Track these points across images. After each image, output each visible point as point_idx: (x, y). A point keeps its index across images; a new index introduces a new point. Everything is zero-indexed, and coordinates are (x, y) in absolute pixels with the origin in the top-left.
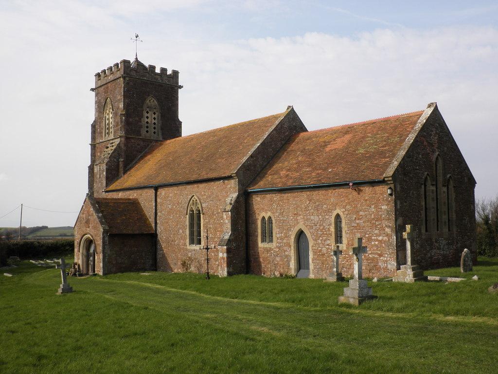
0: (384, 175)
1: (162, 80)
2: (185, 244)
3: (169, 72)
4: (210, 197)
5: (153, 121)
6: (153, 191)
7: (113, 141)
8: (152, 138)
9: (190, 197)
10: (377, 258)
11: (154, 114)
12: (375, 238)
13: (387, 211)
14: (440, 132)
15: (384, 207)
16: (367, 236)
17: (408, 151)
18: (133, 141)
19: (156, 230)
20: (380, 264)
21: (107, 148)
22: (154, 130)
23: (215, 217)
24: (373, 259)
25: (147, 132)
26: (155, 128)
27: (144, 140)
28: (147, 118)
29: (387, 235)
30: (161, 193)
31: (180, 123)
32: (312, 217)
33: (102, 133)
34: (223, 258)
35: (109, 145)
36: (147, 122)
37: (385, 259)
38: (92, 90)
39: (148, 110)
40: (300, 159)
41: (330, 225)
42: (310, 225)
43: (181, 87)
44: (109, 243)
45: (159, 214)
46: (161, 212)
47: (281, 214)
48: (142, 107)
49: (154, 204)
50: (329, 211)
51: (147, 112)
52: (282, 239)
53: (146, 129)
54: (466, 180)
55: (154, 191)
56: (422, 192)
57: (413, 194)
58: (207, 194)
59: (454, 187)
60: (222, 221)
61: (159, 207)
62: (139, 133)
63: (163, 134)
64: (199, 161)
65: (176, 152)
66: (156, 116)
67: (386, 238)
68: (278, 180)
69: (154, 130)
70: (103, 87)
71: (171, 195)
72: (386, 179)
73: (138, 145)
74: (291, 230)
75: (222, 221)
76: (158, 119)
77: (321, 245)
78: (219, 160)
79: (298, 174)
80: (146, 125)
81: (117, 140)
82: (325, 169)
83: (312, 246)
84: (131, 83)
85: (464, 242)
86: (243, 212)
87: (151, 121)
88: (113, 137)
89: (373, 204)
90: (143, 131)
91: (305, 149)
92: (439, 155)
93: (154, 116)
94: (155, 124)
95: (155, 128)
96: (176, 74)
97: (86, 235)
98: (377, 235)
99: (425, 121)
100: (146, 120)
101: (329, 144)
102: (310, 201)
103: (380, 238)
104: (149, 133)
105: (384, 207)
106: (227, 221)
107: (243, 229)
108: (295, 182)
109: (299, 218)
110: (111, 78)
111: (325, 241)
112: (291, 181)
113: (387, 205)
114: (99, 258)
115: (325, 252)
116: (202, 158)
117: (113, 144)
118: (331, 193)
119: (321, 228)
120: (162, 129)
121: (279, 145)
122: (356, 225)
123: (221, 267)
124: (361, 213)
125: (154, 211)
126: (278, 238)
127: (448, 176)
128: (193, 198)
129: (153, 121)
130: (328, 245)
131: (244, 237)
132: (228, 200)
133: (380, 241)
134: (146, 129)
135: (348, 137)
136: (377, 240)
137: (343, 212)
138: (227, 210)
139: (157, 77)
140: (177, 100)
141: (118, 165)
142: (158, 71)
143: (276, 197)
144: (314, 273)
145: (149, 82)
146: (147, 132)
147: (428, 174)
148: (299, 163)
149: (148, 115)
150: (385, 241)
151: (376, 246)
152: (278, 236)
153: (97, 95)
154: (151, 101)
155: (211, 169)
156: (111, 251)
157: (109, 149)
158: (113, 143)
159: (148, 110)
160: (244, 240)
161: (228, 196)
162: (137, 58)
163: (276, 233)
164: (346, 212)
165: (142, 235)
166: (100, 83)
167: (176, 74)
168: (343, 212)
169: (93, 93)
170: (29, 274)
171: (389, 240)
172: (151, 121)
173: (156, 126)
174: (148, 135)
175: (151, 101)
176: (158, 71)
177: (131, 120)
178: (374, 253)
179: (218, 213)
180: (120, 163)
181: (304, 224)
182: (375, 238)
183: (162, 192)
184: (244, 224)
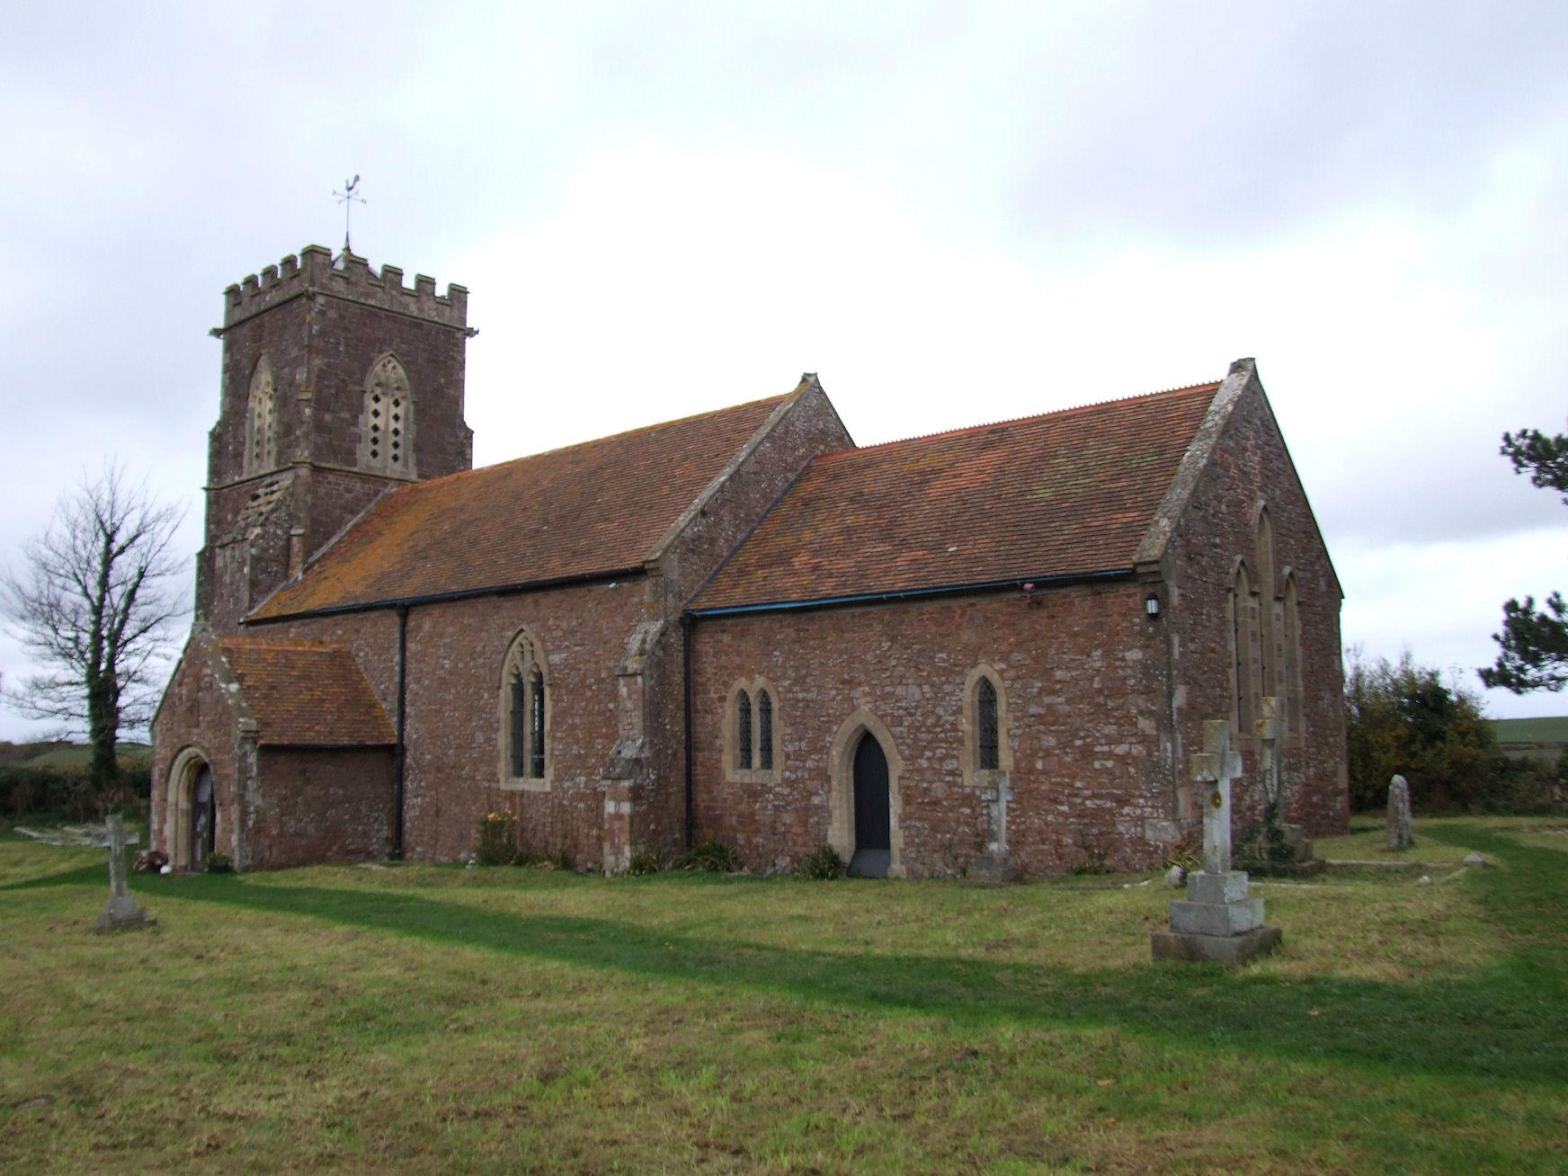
0: (1135, 558)
1: (421, 310)
2: (495, 774)
3: (441, 290)
4: (573, 632)
5: (393, 425)
6: (394, 620)
7: (275, 478)
8: (388, 473)
9: (511, 634)
10: (1110, 809)
11: (397, 403)
12: (1106, 748)
13: (1145, 666)
14: (1266, 444)
15: (1135, 655)
16: (1078, 743)
17: (1195, 490)
18: (331, 478)
19: (401, 736)
20: (1121, 828)
21: (255, 497)
22: (393, 451)
23: (589, 694)
24: (1097, 813)
25: (375, 454)
26: (396, 445)
27: (365, 477)
28: (376, 414)
29: (1144, 739)
30: (419, 627)
31: (469, 434)
32: (900, 691)
33: (241, 455)
34: (618, 816)
35: (261, 491)
36: (375, 428)
37: (1138, 811)
38: (216, 332)
39: (378, 391)
40: (850, 520)
41: (959, 711)
42: (892, 716)
43: (472, 333)
44: (260, 773)
45: (412, 686)
46: (418, 680)
47: (800, 681)
48: (361, 382)
49: (397, 658)
50: (953, 671)
51: (377, 399)
52: (801, 756)
53: (372, 447)
54: (1323, 586)
55: (397, 620)
56: (1230, 616)
57: (1208, 615)
58: (564, 625)
59: (1299, 604)
60: (611, 706)
61: (412, 667)
62: (350, 456)
63: (419, 464)
64: (538, 531)
65: (462, 509)
66: (400, 411)
67: (1138, 750)
68: (789, 582)
69: (393, 451)
70: (248, 325)
71: (450, 630)
72: (1140, 570)
73: (349, 490)
74: (829, 730)
75: (611, 706)
76: (406, 419)
77: (928, 775)
78: (601, 526)
79: (849, 562)
80: (372, 434)
81: (285, 475)
82: (938, 547)
83: (901, 778)
84: (332, 314)
85: (1322, 762)
86: (678, 678)
87: (387, 425)
88: (273, 468)
89: (1097, 647)
90: (363, 451)
91: (861, 494)
92: (1265, 508)
93: (394, 410)
94: (396, 432)
95: (396, 445)
96: (458, 294)
97: (186, 752)
98: (1110, 741)
99: (1230, 408)
100: (373, 421)
101: (936, 479)
102: (893, 639)
103: (1121, 750)
104: (380, 458)
105: (1135, 655)
106: (629, 705)
107: (679, 728)
108: (844, 585)
109: (858, 693)
110: (271, 298)
111: (941, 760)
112: (831, 582)
113: (1144, 647)
114: (226, 820)
115: (940, 795)
116: (546, 522)
117: (275, 487)
118: (962, 616)
119: (930, 721)
120: (418, 448)
121: (780, 484)
122: (1041, 711)
123: (613, 844)
124: (1059, 674)
125: (397, 679)
126: (788, 756)
127: (1287, 570)
128: (519, 639)
129: (393, 425)
130: (952, 773)
131: (682, 754)
132: (634, 643)
133: (1122, 760)
134: (372, 447)
135: (993, 457)
136: (1110, 755)
137: (1001, 672)
138: (630, 671)
139: (406, 299)
140: (463, 368)
141: (288, 547)
142: (409, 283)
143: (785, 632)
144: (904, 860)
145: (382, 314)
146: (375, 454)
147: (1242, 563)
148: (848, 531)
149: (379, 407)
150: (1135, 758)
151: (1109, 772)
152: (790, 748)
153: (229, 348)
154: (389, 369)
155: (575, 553)
156: (264, 796)
157: (261, 501)
158: (272, 484)
159: (378, 391)
160: (682, 763)
161: (630, 630)
162: (348, 249)
163: (783, 741)
164: (1012, 673)
165: (362, 749)
166: (239, 315)
167: (458, 294)
168: (1001, 672)
169: (218, 344)
170: (1108, 880)
171: (1150, 754)
172: (387, 425)
173: (399, 439)
174: (376, 463)
175: (389, 369)
176: (409, 283)
177: (328, 417)
178: (1099, 797)
179: (600, 681)
180: (295, 540)
181: (874, 711)
182: (1106, 748)
183: (424, 623)
184: (681, 714)
